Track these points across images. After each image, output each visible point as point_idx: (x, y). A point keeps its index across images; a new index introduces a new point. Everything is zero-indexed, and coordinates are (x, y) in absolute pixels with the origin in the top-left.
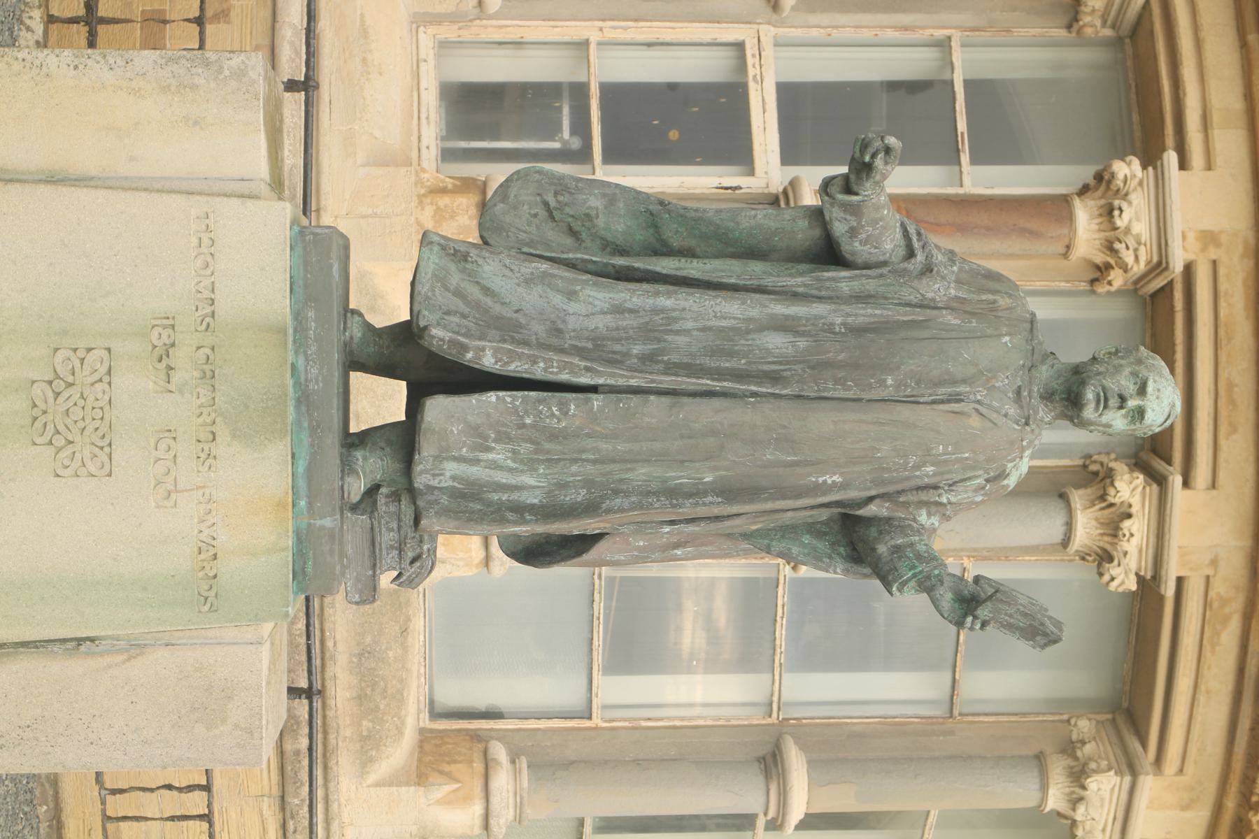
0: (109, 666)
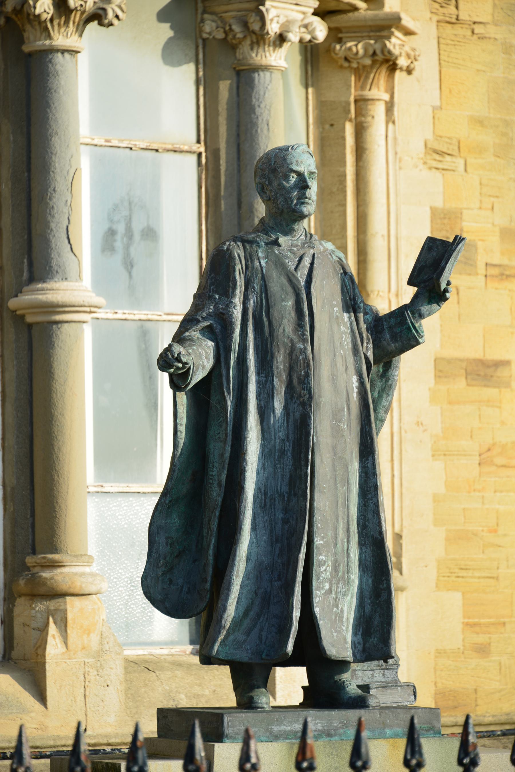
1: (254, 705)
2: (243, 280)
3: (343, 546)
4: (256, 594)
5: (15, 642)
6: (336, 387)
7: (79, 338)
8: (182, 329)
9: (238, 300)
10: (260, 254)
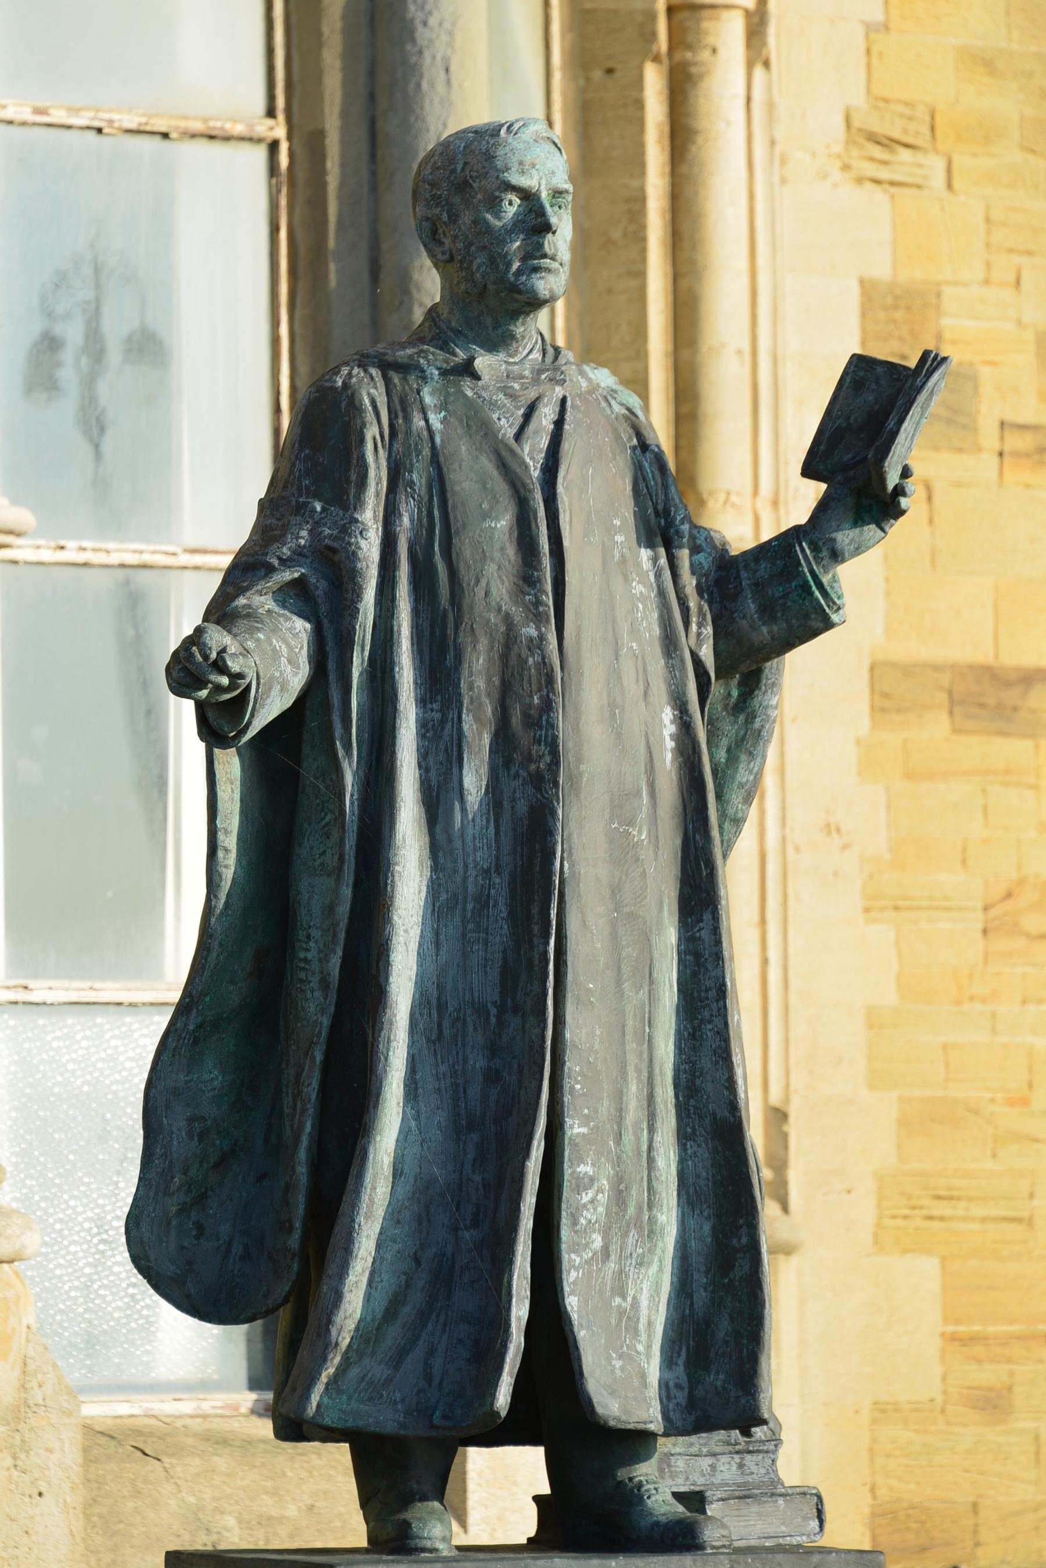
1: (412, 1543)
3: (638, 1139)
4: (417, 1260)
6: (619, 736)
8: (230, 590)
10: (428, 399)
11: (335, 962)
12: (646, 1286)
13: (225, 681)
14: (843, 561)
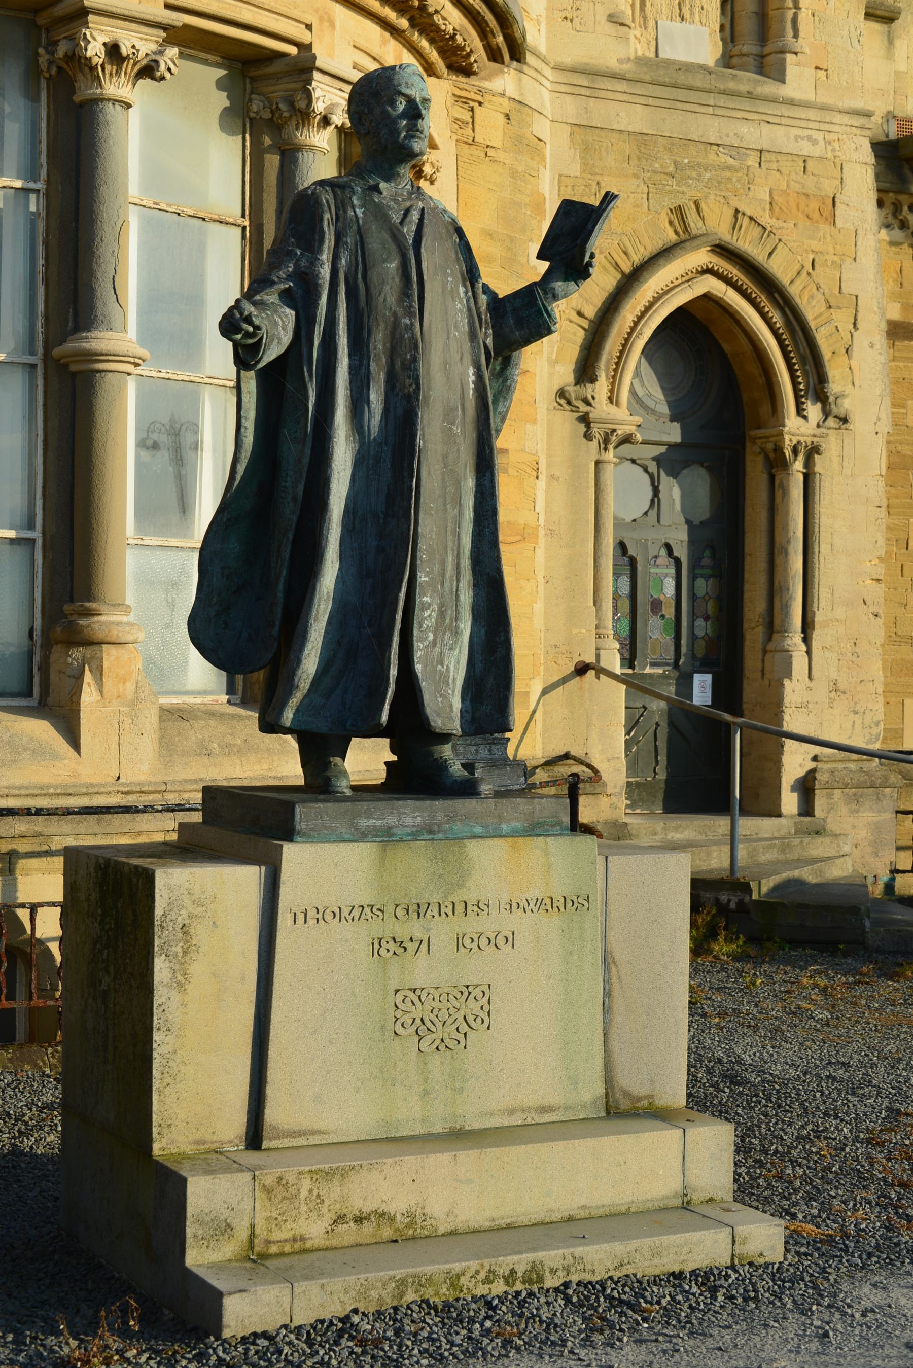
0: (619, 978)
1: (332, 789)
2: (333, 233)
3: (452, 585)
4: (339, 643)
5: (51, 688)
6: (448, 379)
7: (123, 389)
8: (252, 292)
9: (325, 256)
10: (355, 202)
11: (301, 488)
12: (453, 660)
13: (251, 329)
14: (558, 300)
